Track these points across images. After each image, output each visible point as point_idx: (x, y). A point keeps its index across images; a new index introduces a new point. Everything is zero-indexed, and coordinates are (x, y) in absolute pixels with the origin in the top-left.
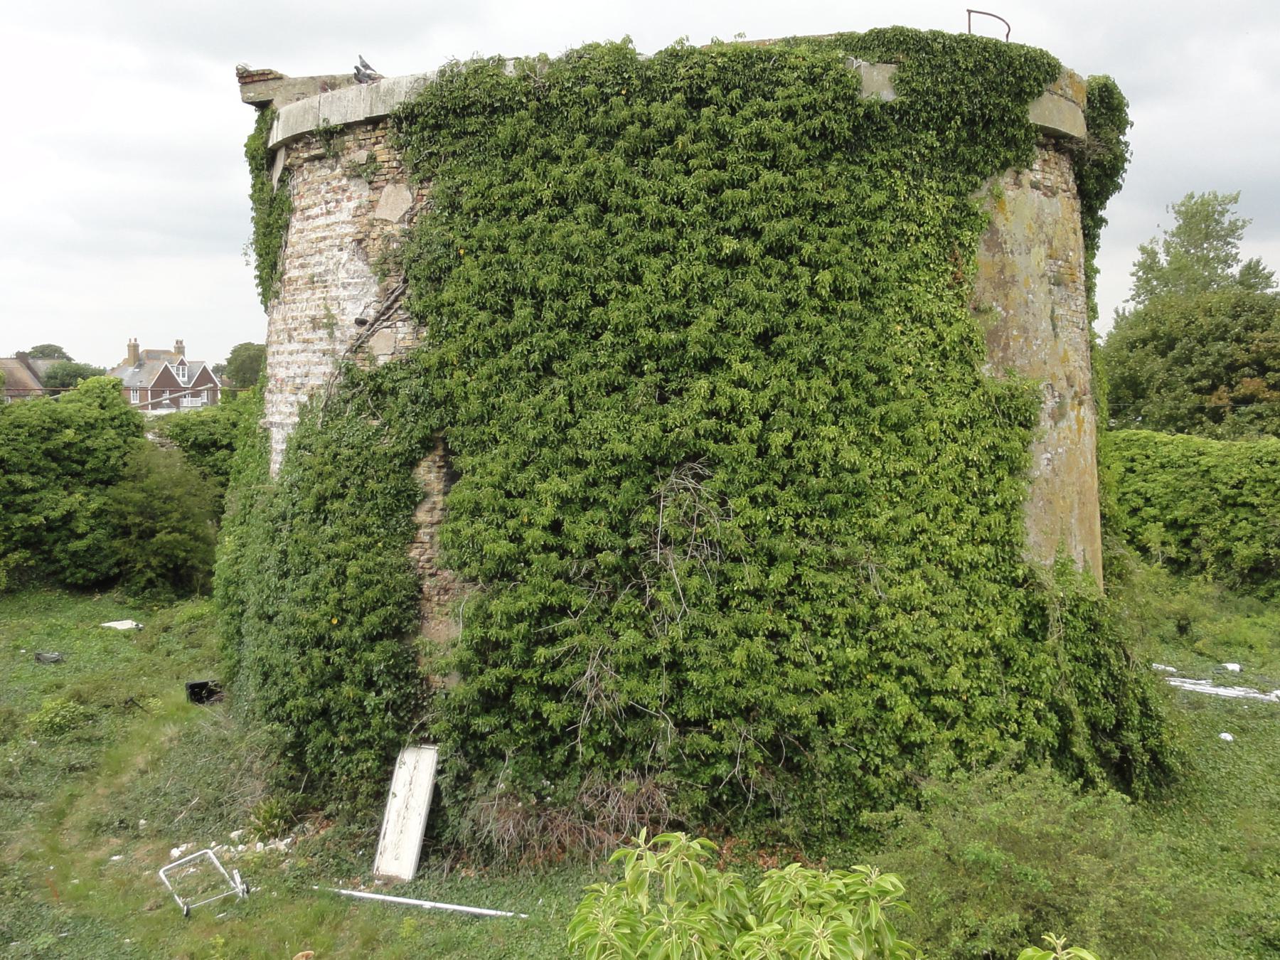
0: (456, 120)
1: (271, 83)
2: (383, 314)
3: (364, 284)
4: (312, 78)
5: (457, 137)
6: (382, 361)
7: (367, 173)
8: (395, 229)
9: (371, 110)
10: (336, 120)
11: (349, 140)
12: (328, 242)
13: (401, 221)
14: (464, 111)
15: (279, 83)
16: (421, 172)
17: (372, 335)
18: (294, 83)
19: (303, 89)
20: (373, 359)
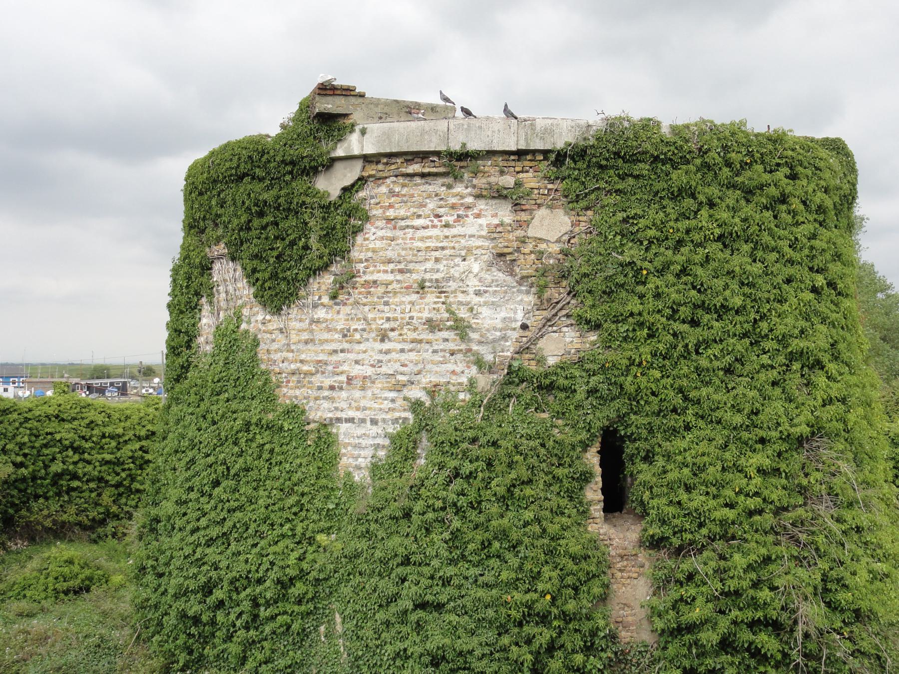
0: (607, 165)
1: (353, 100)
2: (549, 320)
3: (506, 292)
4: (397, 101)
5: (622, 177)
6: (552, 361)
7: (513, 196)
8: (555, 248)
9: (527, 144)
10: (474, 146)
11: (487, 165)
12: (447, 252)
13: (558, 241)
14: (634, 159)
15: (360, 100)
16: (575, 201)
17: (542, 336)
18: (376, 102)
19: (386, 110)
20: (541, 361)
